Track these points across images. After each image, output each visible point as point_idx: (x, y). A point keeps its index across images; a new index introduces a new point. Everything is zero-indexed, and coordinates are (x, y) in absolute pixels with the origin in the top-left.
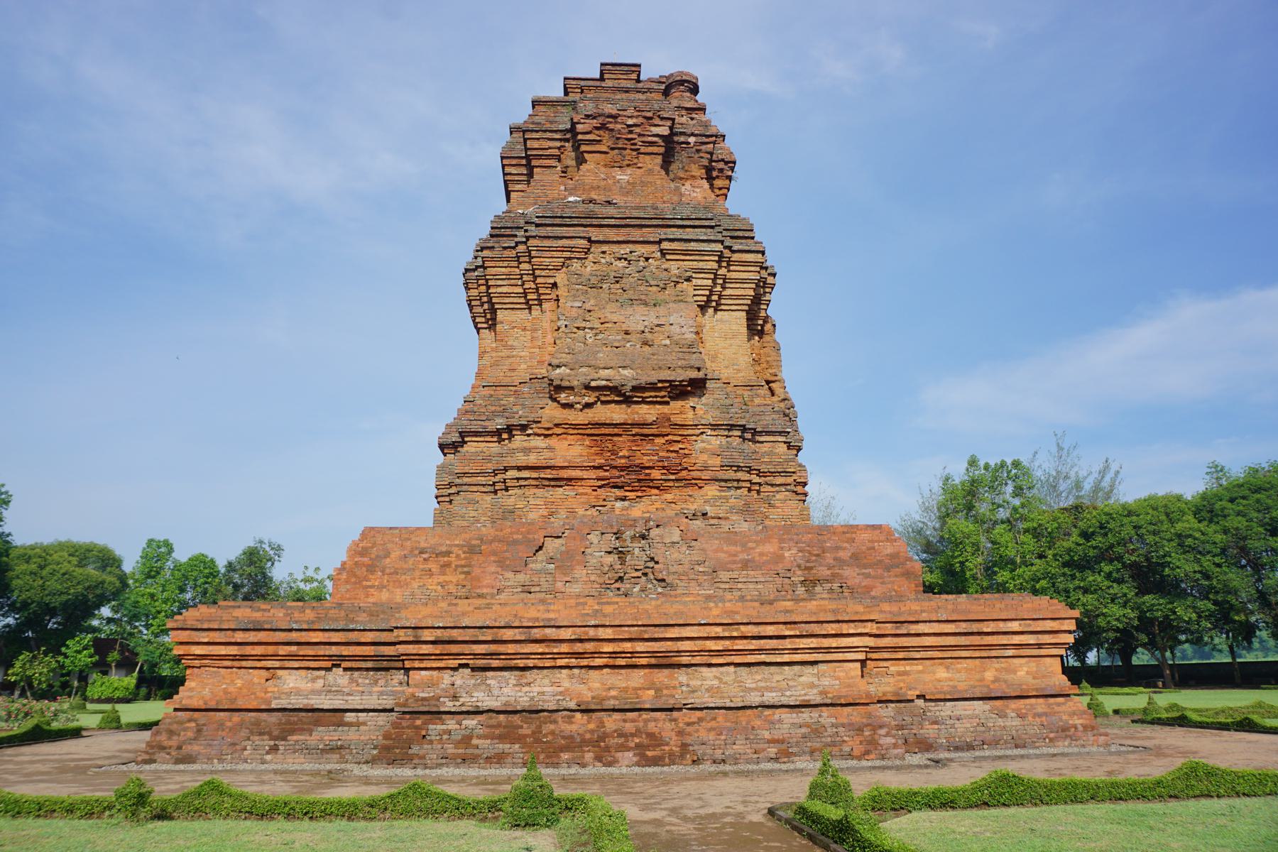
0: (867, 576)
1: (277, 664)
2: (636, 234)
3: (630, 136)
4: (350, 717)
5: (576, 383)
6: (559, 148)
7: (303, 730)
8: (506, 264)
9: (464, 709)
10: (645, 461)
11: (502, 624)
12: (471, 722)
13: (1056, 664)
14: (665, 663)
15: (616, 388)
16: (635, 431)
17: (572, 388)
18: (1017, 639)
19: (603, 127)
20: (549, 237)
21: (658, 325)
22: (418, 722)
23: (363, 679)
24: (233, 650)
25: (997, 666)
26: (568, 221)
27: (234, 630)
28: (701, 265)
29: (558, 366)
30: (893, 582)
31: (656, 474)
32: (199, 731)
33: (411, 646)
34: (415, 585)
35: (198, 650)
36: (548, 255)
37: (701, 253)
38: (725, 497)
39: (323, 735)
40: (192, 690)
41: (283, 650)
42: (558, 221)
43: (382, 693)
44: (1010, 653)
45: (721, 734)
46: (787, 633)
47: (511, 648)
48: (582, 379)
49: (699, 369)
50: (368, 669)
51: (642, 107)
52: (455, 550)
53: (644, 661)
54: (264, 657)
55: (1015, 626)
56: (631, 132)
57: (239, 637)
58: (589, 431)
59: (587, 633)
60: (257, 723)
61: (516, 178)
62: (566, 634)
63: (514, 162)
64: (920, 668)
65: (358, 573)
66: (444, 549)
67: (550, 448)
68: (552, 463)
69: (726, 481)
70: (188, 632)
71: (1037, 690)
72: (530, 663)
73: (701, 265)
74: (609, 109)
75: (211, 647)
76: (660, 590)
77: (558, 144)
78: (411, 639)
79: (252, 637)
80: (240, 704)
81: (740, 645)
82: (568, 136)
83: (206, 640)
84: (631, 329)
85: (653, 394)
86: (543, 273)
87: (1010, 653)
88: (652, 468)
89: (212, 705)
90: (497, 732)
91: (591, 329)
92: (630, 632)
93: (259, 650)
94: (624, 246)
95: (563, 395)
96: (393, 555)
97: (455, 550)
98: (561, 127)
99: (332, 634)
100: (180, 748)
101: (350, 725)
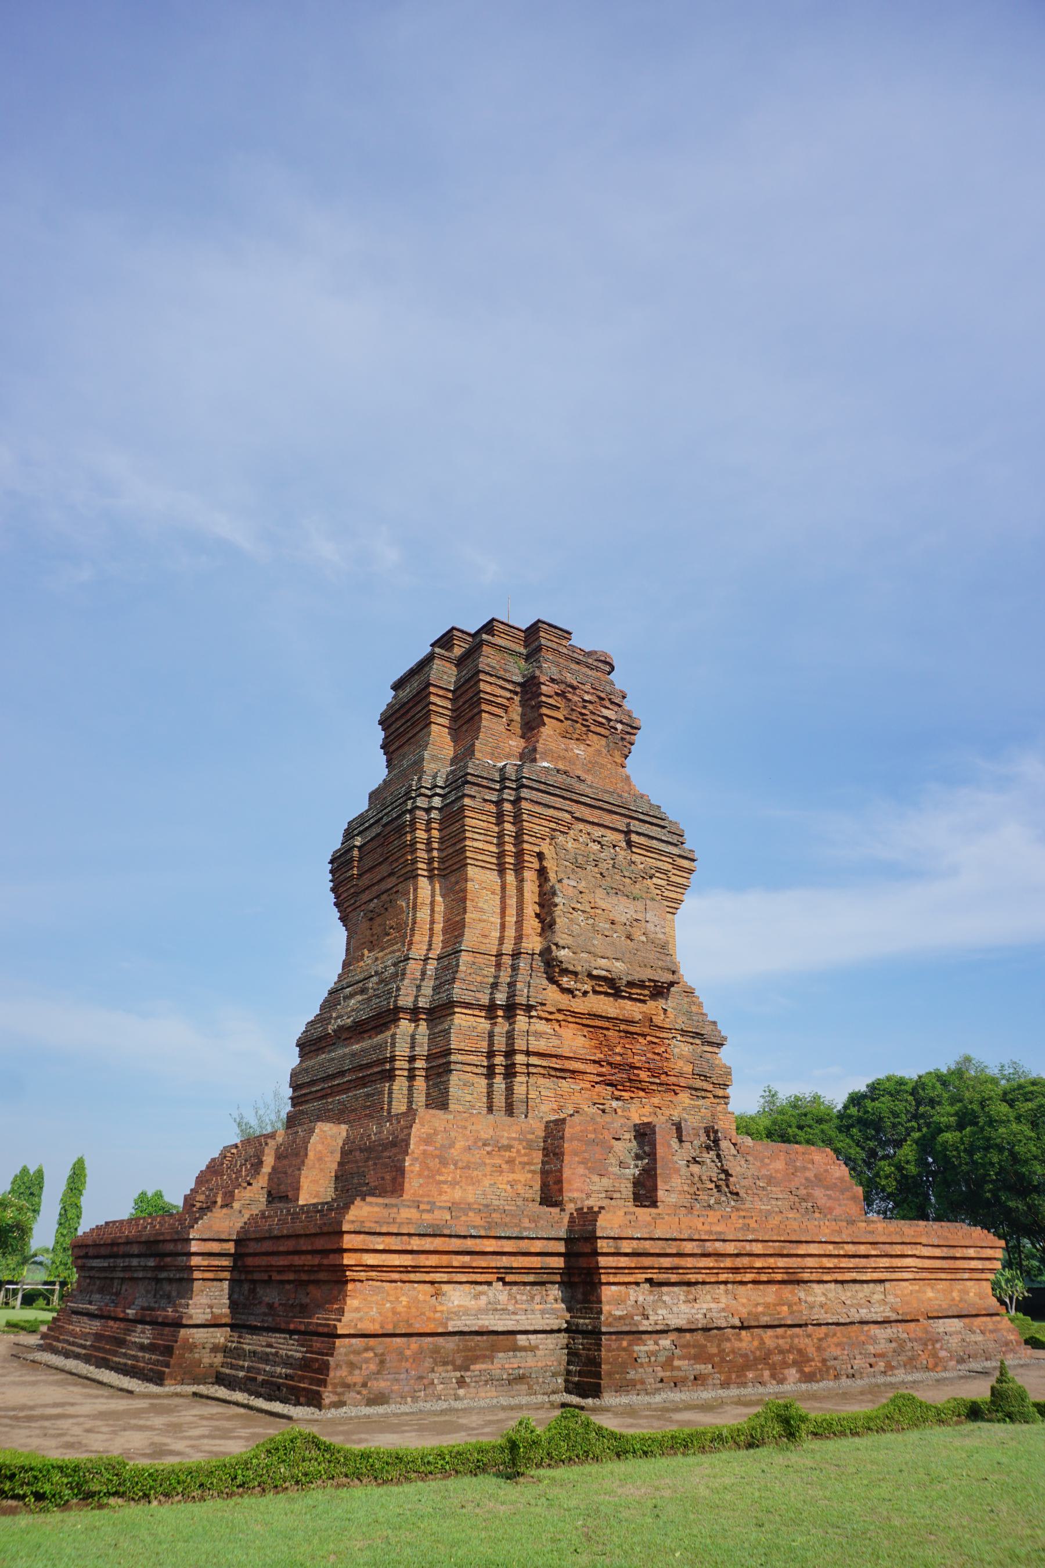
0: (830, 1197)
1: (445, 1277)
2: (607, 819)
3: (583, 711)
4: (522, 1340)
5: (579, 969)
6: (508, 699)
7: (485, 1357)
8: (484, 818)
9: (658, 1328)
10: (637, 1060)
11: (686, 1237)
12: (665, 1342)
13: (987, 1287)
14: (793, 1280)
15: (613, 979)
16: (623, 1027)
17: (576, 974)
18: (974, 1264)
19: (562, 695)
20: (540, 803)
21: (637, 920)
22: (625, 1344)
23: (522, 1294)
24: (407, 1260)
25: (959, 1287)
26: (551, 790)
27: (409, 1235)
28: (659, 864)
29: (564, 948)
30: (846, 1205)
31: (643, 1075)
32: (382, 1362)
33: (611, 1258)
34: (487, 1182)
35: (370, 1259)
36: (537, 821)
37: (660, 852)
38: (699, 1107)
39: (504, 1363)
40: (357, 1310)
41: (457, 1261)
42: (542, 787)
43: (543, 1312)
44: (966, 1276)
45: (844, 1349)
46: (873, 1253)
47: (689, 1262)
48: (586, 965)
49: (674, 972)
50: (525, 1284)
51: (597, 685)
52: (515, 1143)
53: (779, 1277)
54: (435, 1269)
55: (971, 1252)
56: (585, 707)
57: (416, 1244)
58: (585, 1022)
59: (744, 1248)
60: (436, 1350)
61: (441, 710)
62: (730, 1248)
63: (441, 692)
64: (917, 1288)
65: (431, 1165)
66: (505, 1142)
67: (557, 1035)
68: (559, 1051)
69: (696, 1089)
70: (362, 1236)
71: (985, 1309)
72: (700, 1278)
73: (659, 864)
74: (570, 678)
75: (384, 1256)
76: (733, 1203)
77: (508, 695)
78: (612, 1250)
79: (428, 1244)
80: (418, 1327)
81: (845, 1263)
82: (518, 689)
83: (381, 1247)
84: (616, 920)
85: (639, 991)
86: (531, 840)
87: (966, 1276)
88: (639, 1068)
89: (389, 1329)
90: (693, 1351)
91: (583, 912)
92: (774, 1248)
93: (432, 1260)
94: (596, 828)
95: (565, 979)
96: (457, 1146)
97: (515, 1143)
98: (515, 679)
99: (504, 1242)
100: (364, 1385)
101: (524, 1349)
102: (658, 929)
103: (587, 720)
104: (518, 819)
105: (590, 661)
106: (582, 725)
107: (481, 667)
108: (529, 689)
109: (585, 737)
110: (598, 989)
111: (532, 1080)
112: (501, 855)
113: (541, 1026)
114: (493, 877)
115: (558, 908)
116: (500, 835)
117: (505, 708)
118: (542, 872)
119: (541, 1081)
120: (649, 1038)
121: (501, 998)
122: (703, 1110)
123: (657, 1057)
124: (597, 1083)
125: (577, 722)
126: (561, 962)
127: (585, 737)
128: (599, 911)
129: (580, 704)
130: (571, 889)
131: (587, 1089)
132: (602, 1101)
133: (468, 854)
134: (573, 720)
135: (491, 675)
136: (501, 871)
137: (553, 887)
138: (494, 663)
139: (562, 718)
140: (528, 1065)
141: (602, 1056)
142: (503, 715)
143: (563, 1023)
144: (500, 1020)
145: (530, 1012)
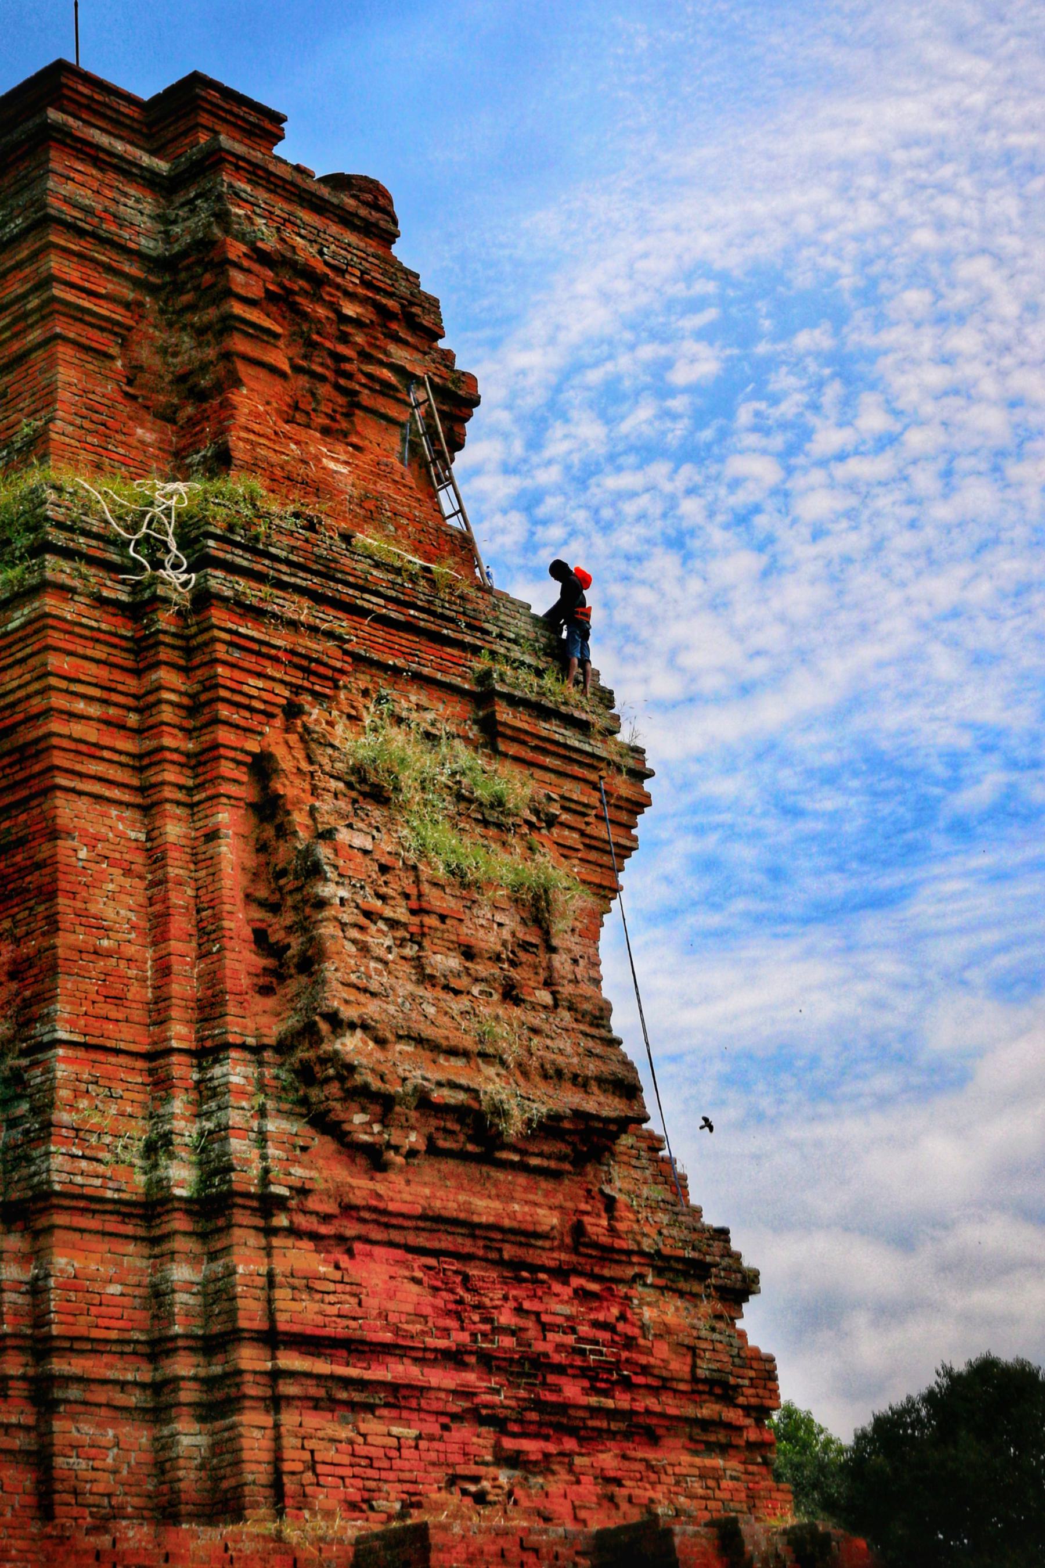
6: (127, 305)
16: (509, 1252)
29: (352, 1026)
56: (344, 338)
58: (421, 1240)
88: (560, 1369)
102: (580, 971)
103: (349, 376)
104: (193, 653)
105: (350, 203)
106: (337, 387)
107: (55, 206)
108: (188, 275)
109: (345, 425)
110: (443, 1143)
111: (289, 1418)
112: (144, 762)
113: (299, 1257)
114: (124, 828)
115: (327, 913)
116: (146, 704)
117: (123, 335)
118: (268, 809)
119: (312, 1421)
120: (576, 1282)
121: (181, 1176)
122: (725, 1483)
123: (604, 1336)
124: (455, 1417)
125: (322, 378)
126: (351, 1069)
127: (345, 425)
128: (432, 921)
129: (331, 329)
130: (359, 857)
131: (431, 1438)
132: (472, 1469)
133: (58, 759)
134: (313, 375)
135: (81, 233)
136: (148, 808)
137: (308, 853)
138: (85, 196)
139: (286, 367)
140: (276, 1375)
141: (464, 1337)
142: (114, 351)
143: (358, 1246)
144: (180, 1244)
145: (267, 1215)
